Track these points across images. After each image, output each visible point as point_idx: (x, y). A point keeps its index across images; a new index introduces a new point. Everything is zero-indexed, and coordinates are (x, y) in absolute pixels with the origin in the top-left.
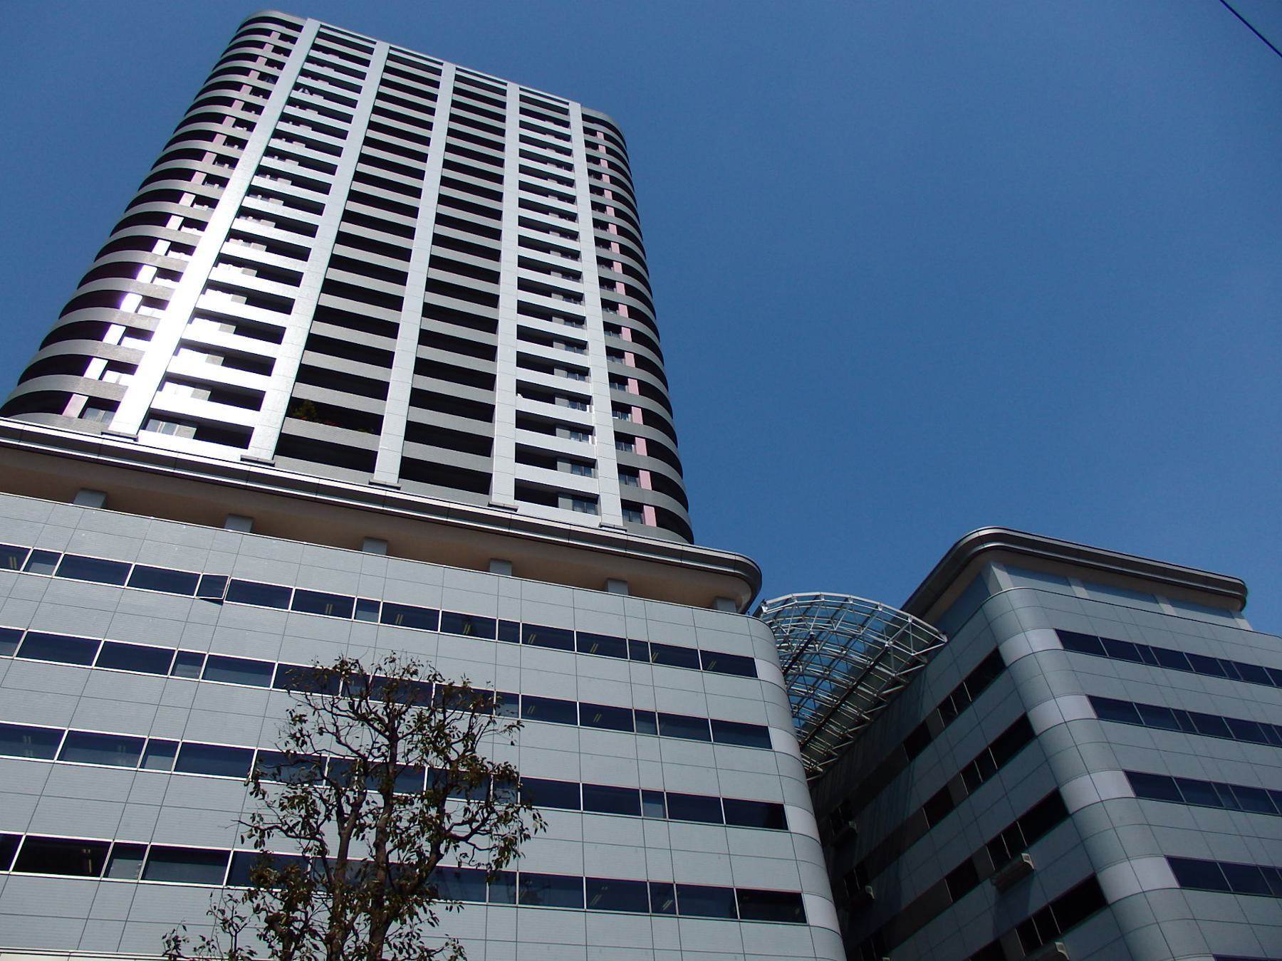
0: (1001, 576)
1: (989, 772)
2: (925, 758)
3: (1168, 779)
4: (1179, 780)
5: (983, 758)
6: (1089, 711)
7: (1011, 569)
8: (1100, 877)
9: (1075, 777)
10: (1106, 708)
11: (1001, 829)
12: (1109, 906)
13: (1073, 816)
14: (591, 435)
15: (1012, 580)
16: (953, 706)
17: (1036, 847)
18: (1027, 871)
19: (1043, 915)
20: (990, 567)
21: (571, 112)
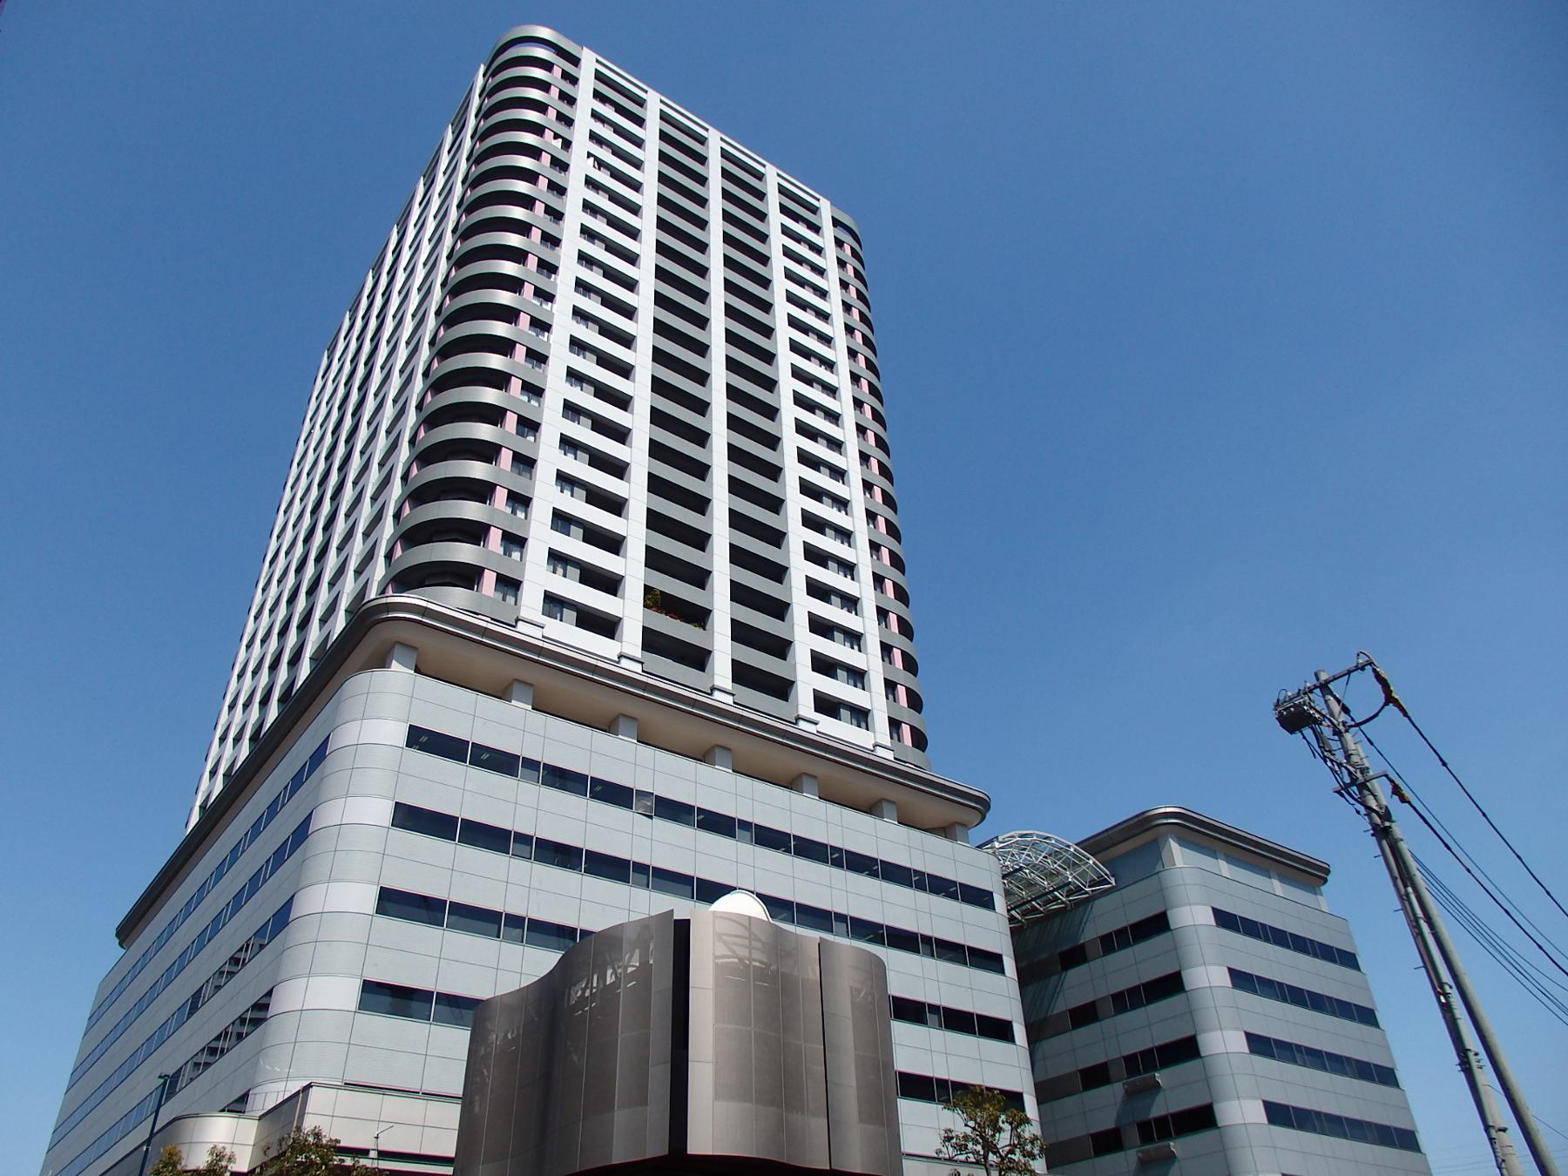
0: (1176, 849)
1: (1124, 944)
2: (1075, 975)
3: (1251, 975)
4: (1275, 1040)
5: (1121, 933)
6: (1242, 1045)
7: (1183, 842)
8: (1169, 913)
9: (1211, 1030)
10: (1241, 979)
11: (1115, 928)
12: (1201, 1057)
13: (1222, 1130)
14: (548, 332)
15: (1183, 855)
16: (1113, 942)
17: (1164, 1071)
18: (1171, 1157)
19: (1162, 1121)
20: (1167, 840)
21: (583, 63)
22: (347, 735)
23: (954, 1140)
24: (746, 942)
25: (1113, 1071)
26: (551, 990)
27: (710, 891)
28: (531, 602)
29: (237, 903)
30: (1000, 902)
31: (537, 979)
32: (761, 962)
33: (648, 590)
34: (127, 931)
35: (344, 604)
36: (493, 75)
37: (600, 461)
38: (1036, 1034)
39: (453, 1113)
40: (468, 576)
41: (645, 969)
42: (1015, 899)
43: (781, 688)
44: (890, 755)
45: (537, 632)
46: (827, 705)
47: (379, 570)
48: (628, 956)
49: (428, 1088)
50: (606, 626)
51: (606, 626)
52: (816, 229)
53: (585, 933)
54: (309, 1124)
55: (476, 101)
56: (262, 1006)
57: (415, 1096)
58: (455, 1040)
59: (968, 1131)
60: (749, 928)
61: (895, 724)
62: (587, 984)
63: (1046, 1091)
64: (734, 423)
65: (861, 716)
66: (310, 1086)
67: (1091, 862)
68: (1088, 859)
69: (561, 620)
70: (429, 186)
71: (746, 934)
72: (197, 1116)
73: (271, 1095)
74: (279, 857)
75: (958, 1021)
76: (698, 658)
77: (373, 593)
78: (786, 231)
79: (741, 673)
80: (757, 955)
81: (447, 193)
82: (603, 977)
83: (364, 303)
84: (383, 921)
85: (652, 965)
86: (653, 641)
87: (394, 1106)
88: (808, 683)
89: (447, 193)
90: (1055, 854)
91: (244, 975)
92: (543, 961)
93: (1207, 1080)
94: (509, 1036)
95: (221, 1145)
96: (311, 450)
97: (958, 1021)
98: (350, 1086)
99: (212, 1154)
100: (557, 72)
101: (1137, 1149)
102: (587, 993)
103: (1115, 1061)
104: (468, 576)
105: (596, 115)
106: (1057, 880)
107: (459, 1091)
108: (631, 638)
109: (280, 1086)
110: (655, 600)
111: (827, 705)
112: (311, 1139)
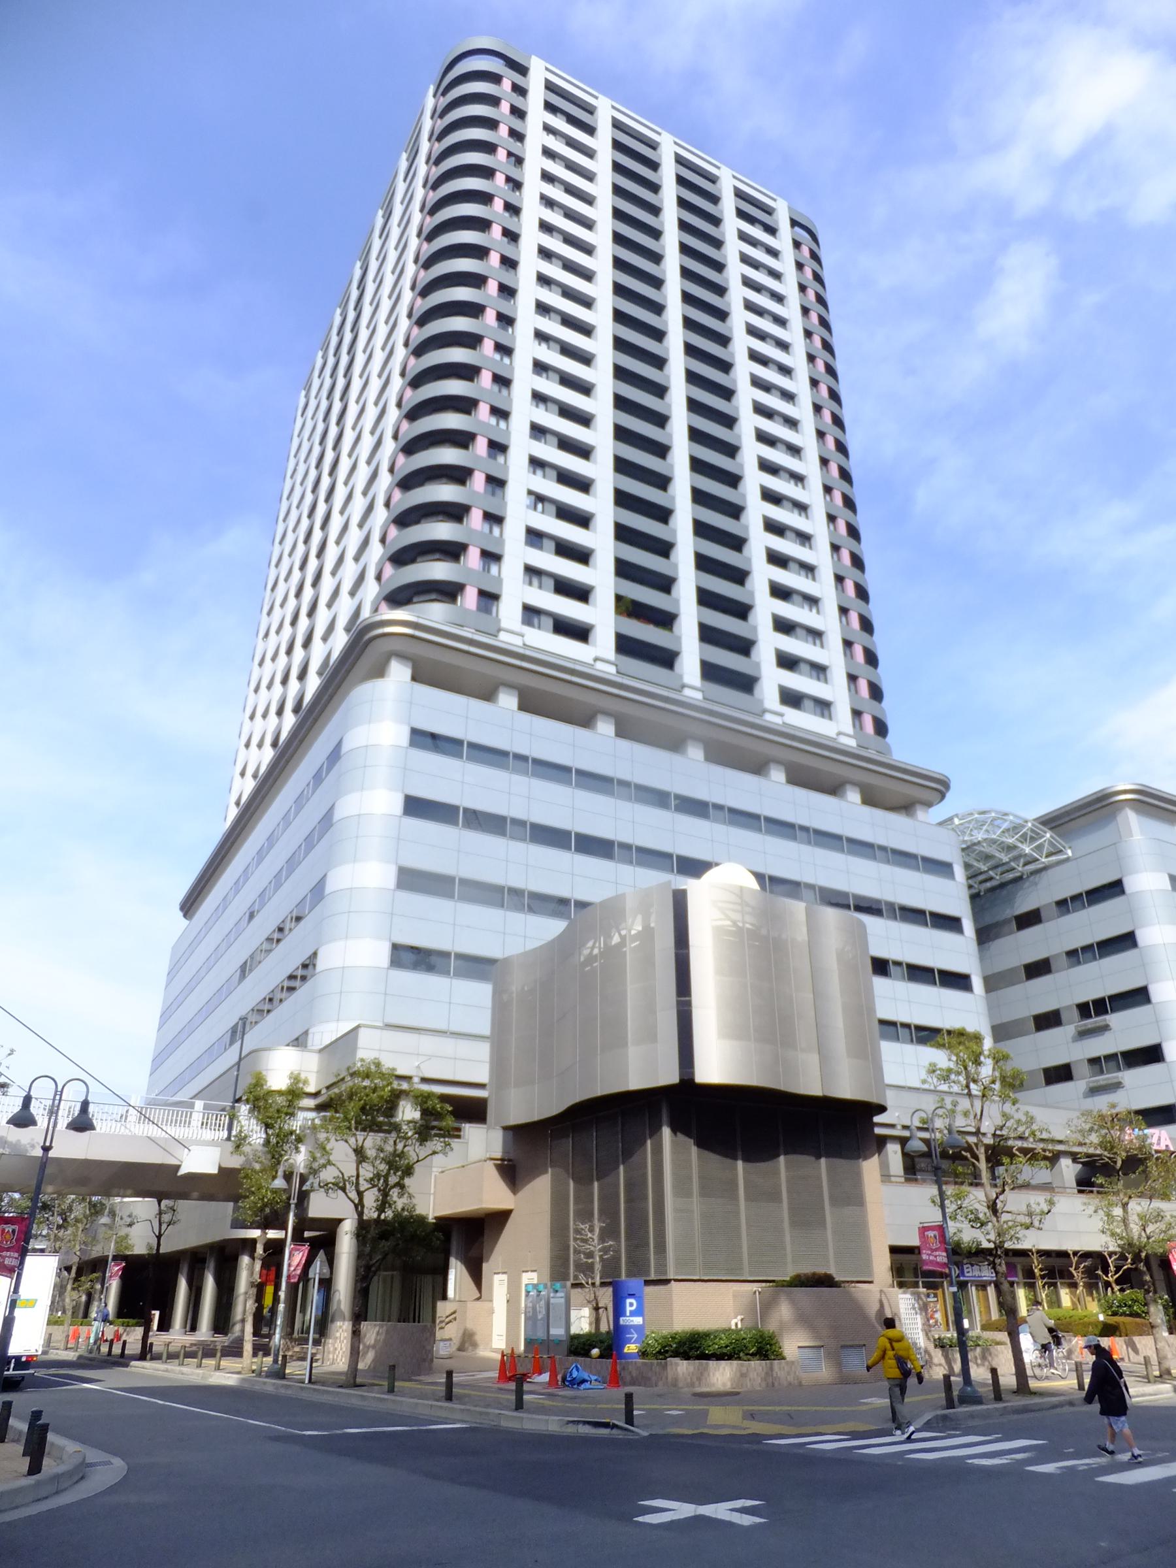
22: (355, 739)
23: (938, 1072)
24: (739, 908)
25: (1064, 1017)
26: (562, 948)
27: (694, 867)
28: (509, 612)
29: (278, 881)
30: (959, 872)
31: (543, 942)
32: (752, 924)
33: (619, 598)
34: (189, 906)
35: (342, 622)
36: (444, 94)
37: (566, 478)
38: (993, 983)
39: (483, 1051)
40: (449, 592)
41: (648, 933)
42: (971, 871)
43: (746, 683)
44: (852, 743)
45: (517, 641)
46: (791, 698)
47: (371, 590)
48: (630, 920)
49: (454, 1028)
50: (580, 632)
51: (580, 632)
52: (771, 230)
53: (582, 905)
54: (361, 1054)
55: (427, 124)
56: (308, 965)
57: (445, 1035)
58: (479, 993)
59: (952, 1065)
60: (741, 897)
61: (857, 714)
62: (594, 943)
63: (1001, 1032)
64: (696, 435)
65: (823, 707)
66: (358, 1027)
67: (1048, 835)
68: (1045, 832)
69: (539, 628)
70: (388, 217)
71: (740, 901)
72: (269, 1049)
73: (325, 1033)
74: (310, 843)
75: (919, 973)
76: (666, 659)
77: (366, 613)
78: (743, 237)
79: (710, 671)
80: (748, 918)
81: (405, 224)
82: (609, 937)
83: (334, 340)
84: (404, 895)
85: (653, 928)
86: (626, 645)
87: (427, 1043)
88: (772, 679)
89: (405, 224)
90: (1015, 829)
91: (289, 940)
92: (551, 928)
93: (1157, 1022)
94: (526, 988)
95: (296, 1072)
96: (298, 486)
97: (919, 973)
98: (389, 1026)
99: (290, 1078)
100: (506, 84)
101: (1087, 1080)
102: (596, 951)
103: (1068, 1008)
104: (449, 592)
105: (548, 129)
106: (1015, 853)
107: (486, 1030)
108: (604, 643)
109: (332, 1026)
110: (627, 608)
111: (791, 698)
112: (373, 1067)
